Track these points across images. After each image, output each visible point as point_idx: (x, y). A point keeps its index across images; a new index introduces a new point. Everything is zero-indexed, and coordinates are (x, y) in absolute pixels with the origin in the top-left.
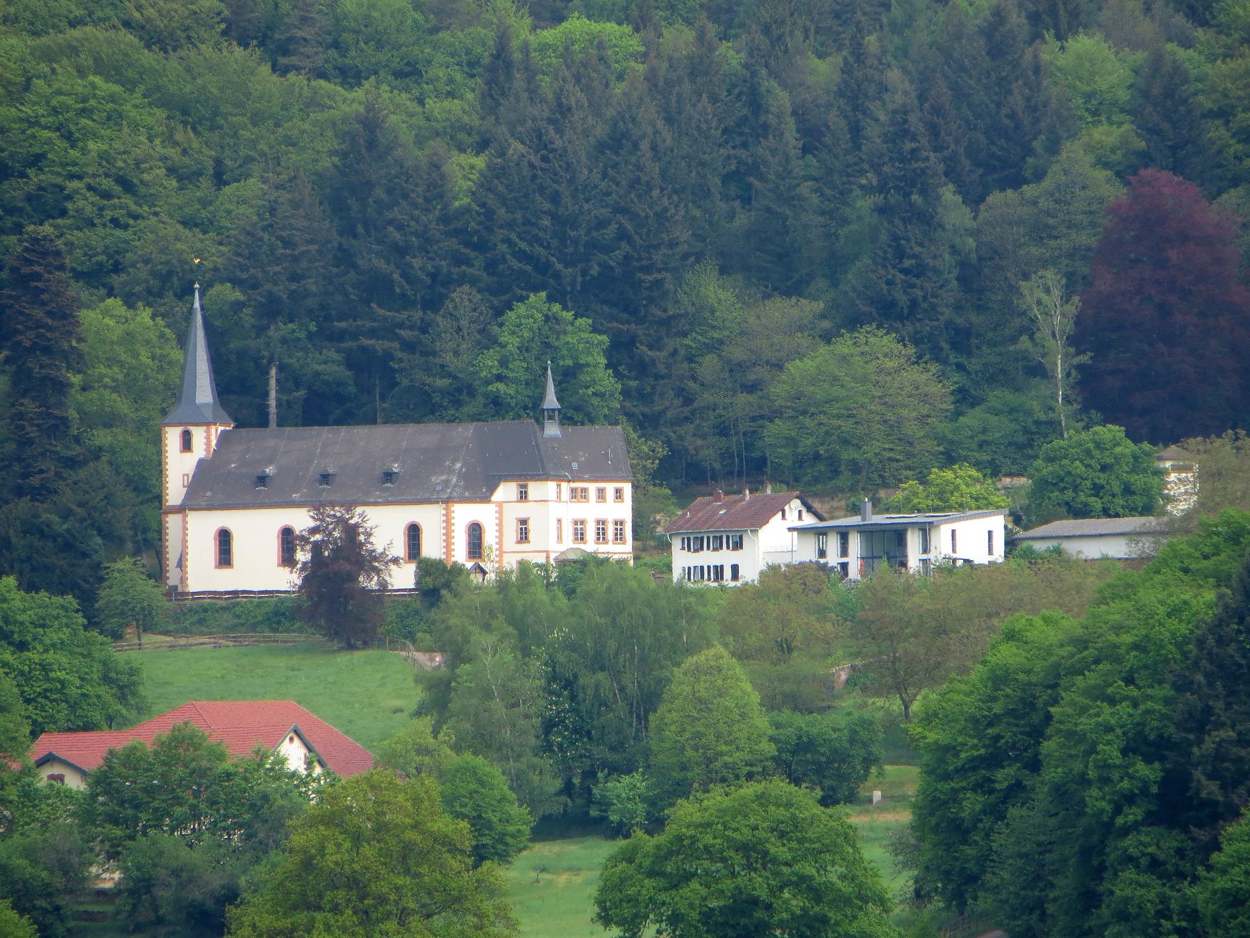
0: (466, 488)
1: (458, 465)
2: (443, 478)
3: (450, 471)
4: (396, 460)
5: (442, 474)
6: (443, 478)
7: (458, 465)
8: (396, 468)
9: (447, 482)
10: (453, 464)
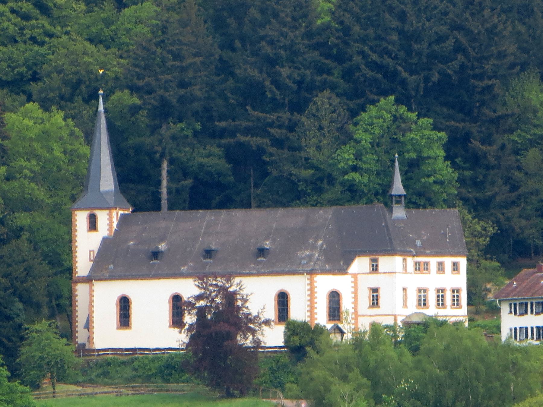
0: (327, 261)
1: (320, 242)
2: (307, 253)
4: (267, 238)
5: (306, 249)
6: (307, 253)
8: (267, 245)
9: (310, 257)
10: (316, 241)
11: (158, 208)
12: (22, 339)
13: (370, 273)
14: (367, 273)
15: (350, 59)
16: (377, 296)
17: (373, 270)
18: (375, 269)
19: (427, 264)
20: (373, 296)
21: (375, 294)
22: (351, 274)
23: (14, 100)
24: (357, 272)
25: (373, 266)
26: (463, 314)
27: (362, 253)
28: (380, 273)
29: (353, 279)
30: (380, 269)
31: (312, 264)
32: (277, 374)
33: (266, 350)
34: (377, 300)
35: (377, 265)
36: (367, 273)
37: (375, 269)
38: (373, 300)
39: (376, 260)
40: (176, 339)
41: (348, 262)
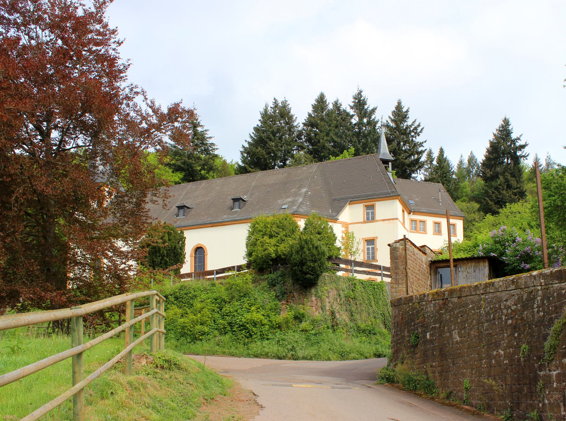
1: (304, 190)
3: (296, 194)
4: (245, 194)
7: (304, 190)
8: (245, 197)
9: (293, 203)
11: (237, 266)
12: (314, 157)
13: (365, 222)
14: (361, 223)
15: (319, 142)
16: (373, 249)
17: (368, 218)
18: (370, 218)
19: (424, 222)
20: (368, 249)
21: (370, 247)
22: (340, 223)
23: (241, 321)
24: (349, 222)
25: (368, 214)
26: (236, 263)
27: (354, 200)
28: (377, 221)
29: (344, 229)
30: (378, 217)
31: (295, 207)
32: (227, 308)
33: (380, 272)
34: (373, 253)
35: (373, 214)
36: (361, 223)
37: (370, 218)
38: (368, 254)
39: (372, 207)
40: (462, 185)
41: (339, 210)
